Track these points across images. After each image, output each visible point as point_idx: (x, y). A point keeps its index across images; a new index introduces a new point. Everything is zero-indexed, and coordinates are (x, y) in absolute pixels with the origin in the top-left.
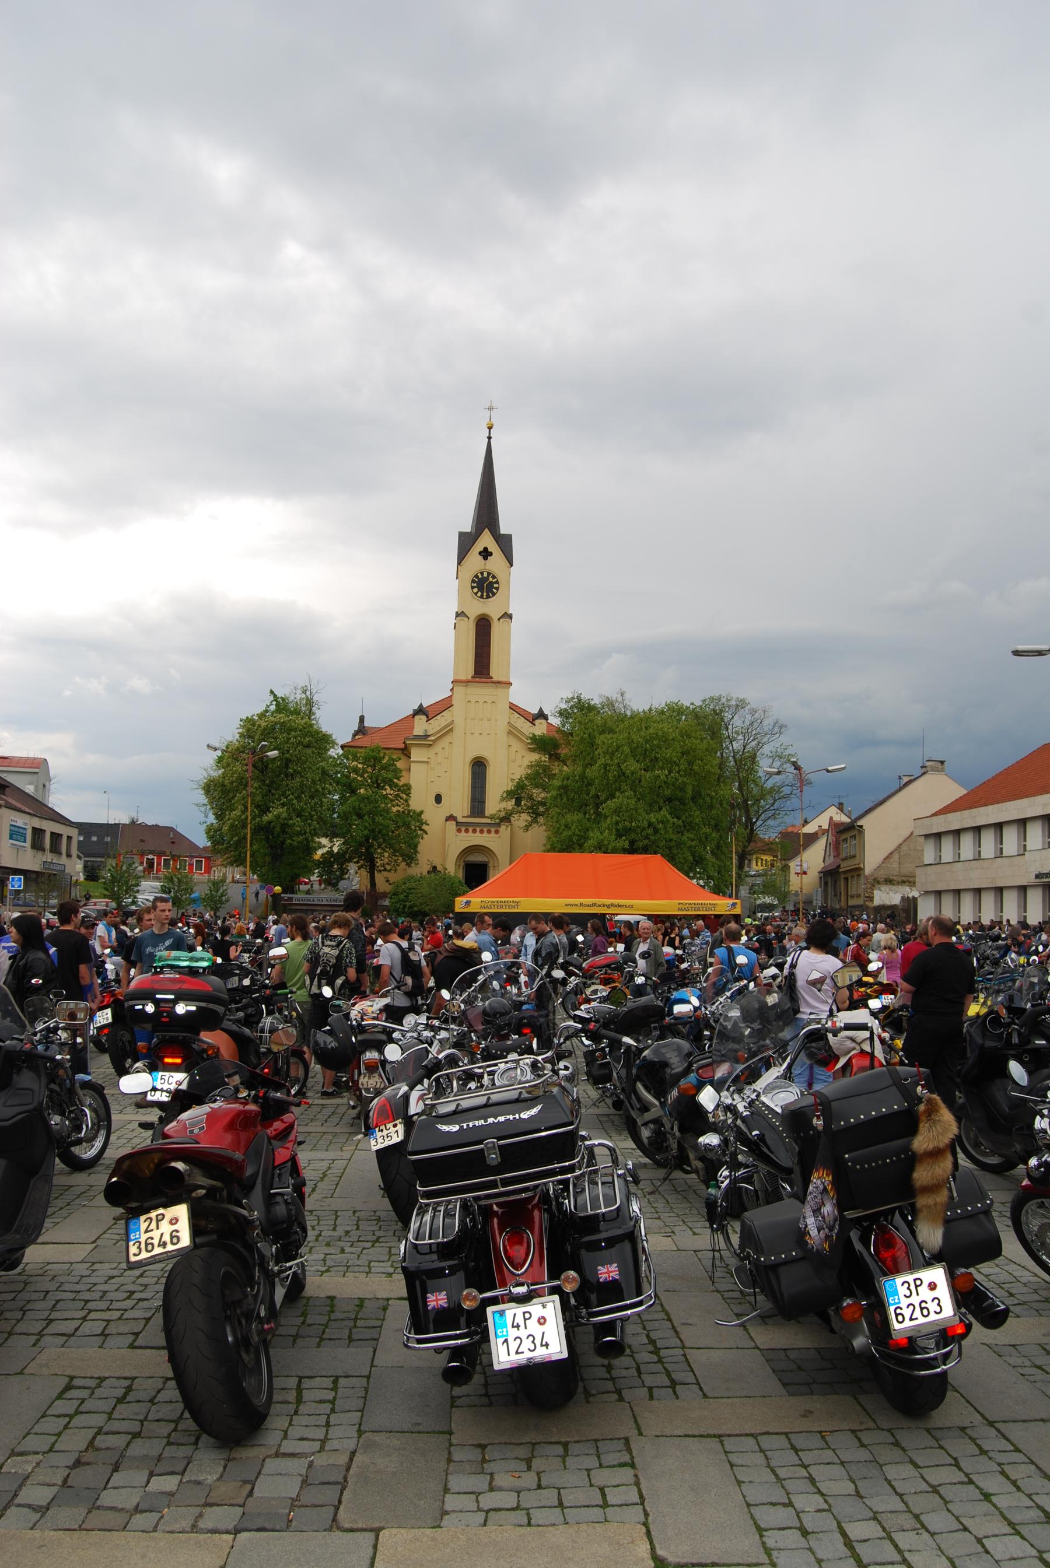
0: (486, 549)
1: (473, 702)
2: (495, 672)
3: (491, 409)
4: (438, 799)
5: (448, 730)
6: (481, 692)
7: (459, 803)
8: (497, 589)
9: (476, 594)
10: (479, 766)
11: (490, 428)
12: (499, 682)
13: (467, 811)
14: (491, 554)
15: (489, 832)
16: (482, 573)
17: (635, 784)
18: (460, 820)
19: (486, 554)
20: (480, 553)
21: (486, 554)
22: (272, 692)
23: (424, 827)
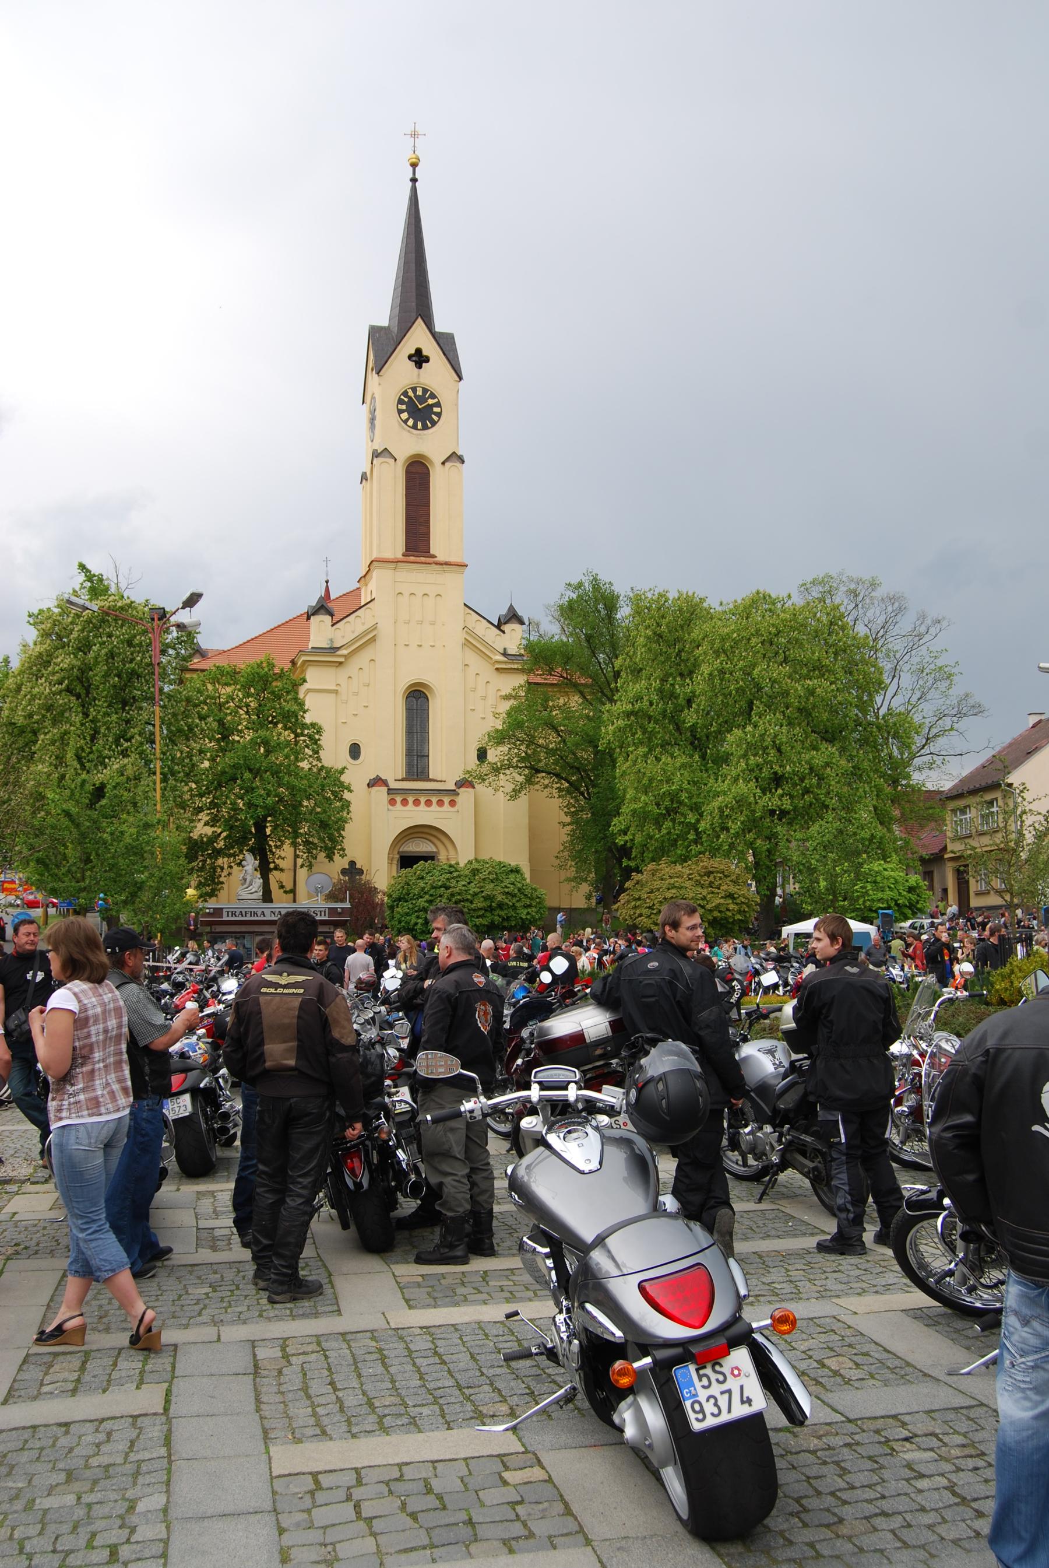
0: (419, 351)
1: (406, 594)
2: (439, 545)
3: (414, 135)
4: (355, 751)
5: (369, 639)
6: (417, 578)
7: (386, 756)
8: (439, 415)
9: (406, 422)
10: (417, 698)
11: (414, 165)
12: (446, 564)
13: (400, 771)
14: (427, 360)
15: (440, 803)
16: (414, 390)
17: (777, 700)
18: (393, 785)
19: (419, 359)
20: (410, 357)
21: (419, 359)
22: (82, 567)
23: (346, 795)
